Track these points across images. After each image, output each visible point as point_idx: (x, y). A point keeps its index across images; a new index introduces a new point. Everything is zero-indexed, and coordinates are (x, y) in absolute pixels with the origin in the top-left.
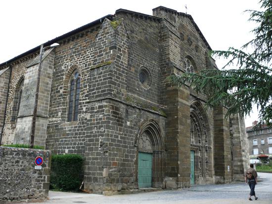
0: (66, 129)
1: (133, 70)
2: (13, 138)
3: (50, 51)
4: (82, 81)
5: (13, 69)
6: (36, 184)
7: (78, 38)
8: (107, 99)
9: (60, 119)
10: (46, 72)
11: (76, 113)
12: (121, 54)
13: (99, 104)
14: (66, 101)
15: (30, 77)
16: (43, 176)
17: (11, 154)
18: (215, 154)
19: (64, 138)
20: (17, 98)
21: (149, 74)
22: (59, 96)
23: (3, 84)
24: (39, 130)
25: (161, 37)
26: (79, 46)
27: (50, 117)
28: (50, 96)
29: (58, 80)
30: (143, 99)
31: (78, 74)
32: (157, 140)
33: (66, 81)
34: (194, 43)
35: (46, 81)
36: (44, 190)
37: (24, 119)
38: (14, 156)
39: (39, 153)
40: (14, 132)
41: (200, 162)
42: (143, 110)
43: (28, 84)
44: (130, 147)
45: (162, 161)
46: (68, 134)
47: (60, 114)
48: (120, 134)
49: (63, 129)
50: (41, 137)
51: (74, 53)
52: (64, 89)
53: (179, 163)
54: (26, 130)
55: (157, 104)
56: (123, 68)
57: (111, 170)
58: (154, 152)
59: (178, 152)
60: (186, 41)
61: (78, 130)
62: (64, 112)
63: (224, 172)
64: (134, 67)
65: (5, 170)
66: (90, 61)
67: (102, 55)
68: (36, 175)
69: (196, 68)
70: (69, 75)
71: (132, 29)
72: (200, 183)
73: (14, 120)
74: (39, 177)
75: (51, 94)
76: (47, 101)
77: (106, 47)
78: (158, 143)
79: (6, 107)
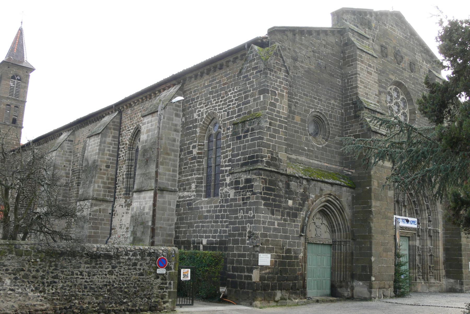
0: (203, 209)
1: (298, 119)
2: (129, 219)
3: (176, 90)
4: (224, 138)
5: (124, 115)
6: (160, 292)
7: (215, 71)
8: (256, 169)
9: (195, 193)
10: (171, 122)
11: (217, 186)
12: (277, 100)
13: (245, 176)
14: (201, 167)
15: (148, 131)
16: (168, 282)
17: (127, 254)
18: (446, 243)
19: (200, 222)
20: (132, 160)
21: (326, 122)
22: (192, 159)
23: (111, 138)
24: (164, 209)
25: (344, 59)
26: (217, 83)
27: (180, 190)
28: (178, 159)
29: (189, 134)
30: (316, 162)
31: (218, 125)
32: (339, 224)
33: (200, 137)
34: (406, 58)
35: (172, 136)
36: (170, 300)
37: (143, 195)
38: (130, 256)
39: (161, 251)
40: (130, 211)
41: (419, 255)
42: (313, 180)
43: (146, 141)
44: (293, 238)
45: (346, 256)
46: (206, 217)
47: (193, 186)
48: (277, 219)
49: (198, 208)
50: (168, 220)
51: (211, 93)
52: (199, 149)
53: (373, 259)
54: (147, 210)
55: (340, 168)
56: (280, 121)
57: (263, 272)
58: (334, 242)
59: (371, 243)
60: (391, 57)
61: (220, 211)
62: (199, 182)
63: (462, 273)
64: (299, 114)
65: (120, 275)
66: (233, 108)
67: (248, 102)
68: (159, 281)
69: (412, 99)
70: (205, 128)
71: (294, 55)
72: (419, 289)
73: (129, 192)
74: (162, 284)
75: (180, 155)
76: (175, 166)
77: (253, 90)
78: (340, 229)
79: (116, 174)
